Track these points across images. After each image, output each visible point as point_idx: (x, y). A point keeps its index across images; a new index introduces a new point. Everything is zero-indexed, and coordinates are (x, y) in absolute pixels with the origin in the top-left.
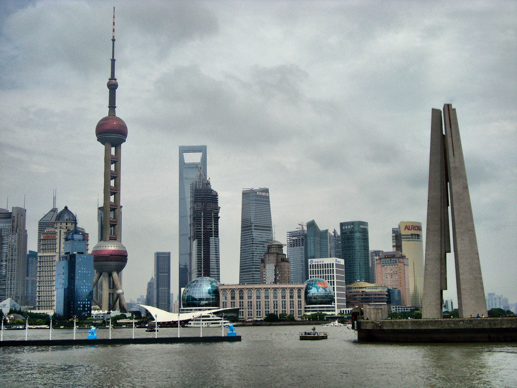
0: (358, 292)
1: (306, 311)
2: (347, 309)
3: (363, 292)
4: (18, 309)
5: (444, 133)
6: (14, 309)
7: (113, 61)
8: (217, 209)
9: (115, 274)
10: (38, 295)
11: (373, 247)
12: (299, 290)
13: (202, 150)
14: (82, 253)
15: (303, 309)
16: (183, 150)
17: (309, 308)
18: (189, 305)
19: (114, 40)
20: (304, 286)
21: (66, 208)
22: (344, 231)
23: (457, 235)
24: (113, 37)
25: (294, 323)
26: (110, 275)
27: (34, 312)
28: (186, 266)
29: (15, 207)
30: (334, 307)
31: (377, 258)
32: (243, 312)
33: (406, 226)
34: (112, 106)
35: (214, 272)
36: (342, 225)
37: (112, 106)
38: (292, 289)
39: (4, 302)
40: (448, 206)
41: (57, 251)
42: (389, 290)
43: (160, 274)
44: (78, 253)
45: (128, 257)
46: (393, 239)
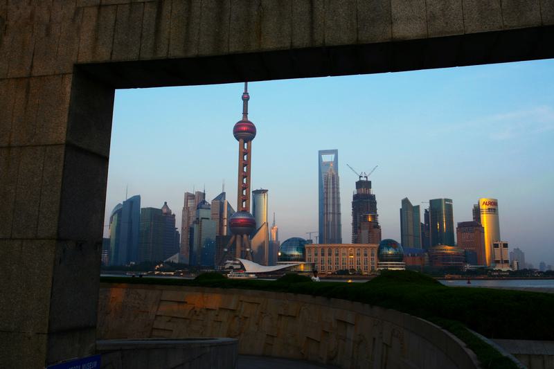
3: (442, 253)
8: (376, 203)
13: (335, 152)
16: (321, 153)
17: (381, 264)
23: (270, 44)
26: (242, 236)
34: (245, 113)
36: (431, 202)
37: (245, 113)
39: (175, 256)
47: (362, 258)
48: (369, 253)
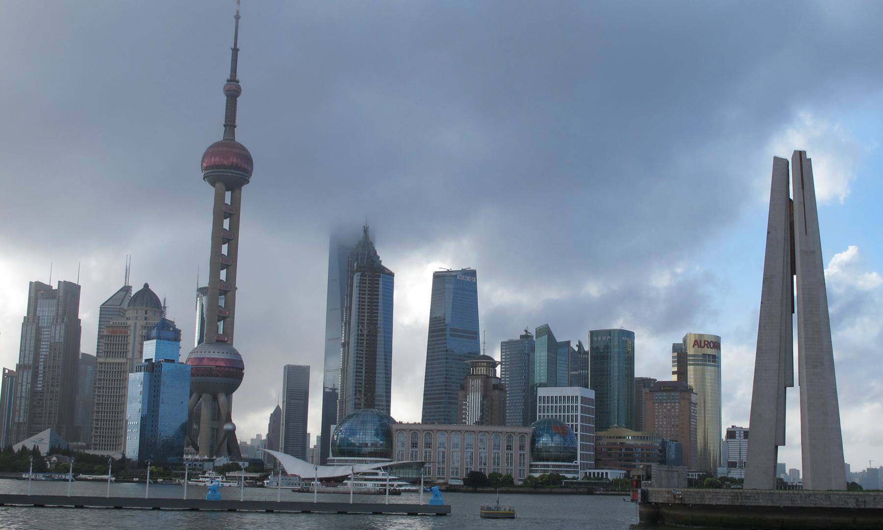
0: (616, 444)
1: (531, 471)
2: (596, 471)
4: (64, 447)
5: (791, 197)
6: (57, 447)
7: (235, 51)
9: (222, 398)
10: (94, 425)
11: (641, 371)
12: (522, 436)
14: (173, 361)
15: (526, 468)
17: (537, 466)
18: (342, 453)
19: (237, 17)
20: (529, 430)
21: (146, 286)
22: (595, 346)
24: (238, 12)
25: (512, 489)
26: (215, 398)
27: (91, 452)
28: (334, 390)
29: (34, 281)
30: (577, 467)
31: (647, 390)
32: (429, 468)
33: (696, 341)
34: (230, 124)
35: (381, 401)
37: (230, 124)
38: (510, 436)
40: (793, 312)
41: (130, 355)
42: (664, 443)
43: (292, 401)
44: (166, 361)
45: (244, 371)
46: (673, 362)
47: (503, 453)
48: (516, 444)
